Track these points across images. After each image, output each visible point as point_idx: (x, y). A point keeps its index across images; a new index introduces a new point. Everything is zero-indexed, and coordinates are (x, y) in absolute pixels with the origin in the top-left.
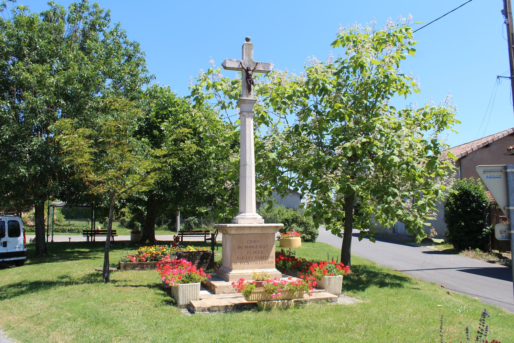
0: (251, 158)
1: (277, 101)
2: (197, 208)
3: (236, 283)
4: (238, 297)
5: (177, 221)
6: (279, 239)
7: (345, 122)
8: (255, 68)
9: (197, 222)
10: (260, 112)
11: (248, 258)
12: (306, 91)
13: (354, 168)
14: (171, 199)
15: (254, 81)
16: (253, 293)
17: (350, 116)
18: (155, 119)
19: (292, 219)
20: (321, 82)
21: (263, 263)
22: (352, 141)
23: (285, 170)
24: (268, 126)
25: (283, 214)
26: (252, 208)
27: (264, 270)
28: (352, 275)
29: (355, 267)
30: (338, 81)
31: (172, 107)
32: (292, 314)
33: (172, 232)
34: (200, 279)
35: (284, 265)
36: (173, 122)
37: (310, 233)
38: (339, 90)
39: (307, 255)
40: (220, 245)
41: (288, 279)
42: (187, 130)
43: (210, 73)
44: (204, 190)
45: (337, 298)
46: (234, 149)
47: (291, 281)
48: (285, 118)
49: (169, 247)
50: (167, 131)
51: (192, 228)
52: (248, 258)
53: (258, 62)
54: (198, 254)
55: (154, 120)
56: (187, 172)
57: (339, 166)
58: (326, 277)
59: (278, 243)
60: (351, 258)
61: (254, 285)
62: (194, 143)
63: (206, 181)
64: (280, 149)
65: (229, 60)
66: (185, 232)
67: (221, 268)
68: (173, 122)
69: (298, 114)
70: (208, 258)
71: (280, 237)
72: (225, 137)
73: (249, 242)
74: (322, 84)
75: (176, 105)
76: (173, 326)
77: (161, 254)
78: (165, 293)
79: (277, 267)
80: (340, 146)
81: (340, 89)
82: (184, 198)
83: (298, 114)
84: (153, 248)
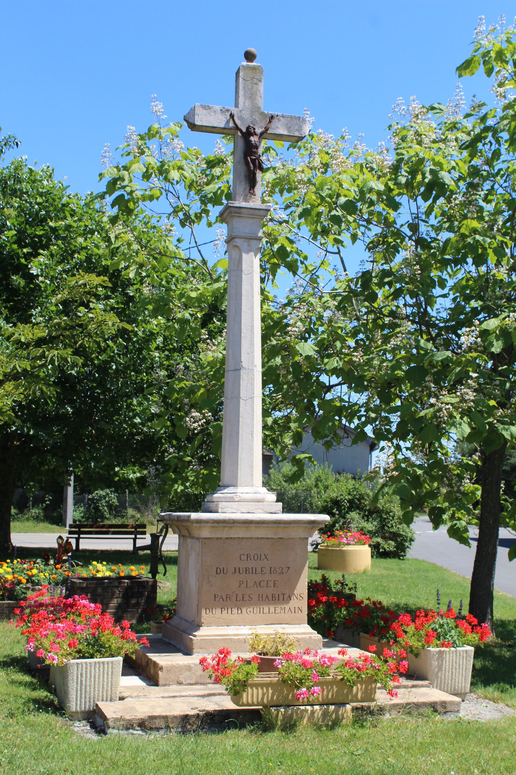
0: (251, 353)
1: (319, 215)
2: (117, 469)
3: (209, 661)
4: (214, 695)
5: (66, 498)
6: (316, 548)
7: (488, 267)
8: (267, 129)
9: (115, 501)
10: (276, 240)
11: (240, 597)
12: (393, 190)
13: (505, 382)
14: (52, 447)
15: (263, 158)
16: (252, 686)
17: (499, 252)
18: (15, 246)
19: (349, 501)
20: (428, 167)
21: (278, 610)
22: (504, 315)
23: (334, 380)
24: (295, 273)
25: (326, 488)
26: (252, 475)
27: (280, 629)
28: (496, 645)
29: (503, 624)
30: (473, 163)
31: (57, 218)
32: (348, 741)
33: (54, 526)
34: (122, 648)
35: (329, 614)
36: (62, 255)
37: (394, 536)
38: (472, 186)
39: (385, 591)
40: (173, 561)
41: (339, 653)
42: (94, 279)
43: (154, 136)
44: (135, 424)
45: (458, 704)
46: (211, 325)
47: (346, 658)
48: (339, 253)
49: (47, 564)
50: (46, 277)
51: (103, 517)
52: (240, 597)
53: (275, 113)
54: (116, 584)
55: (13, 250)
56: (95, 380)
57: (471, 378)
58: (433, 649)
59: (313, 559)
60: (495, 603)
61: (255, 665)
62: (113, 309)
63: (140, 404)
64: (323, 332)
65: (204, 107)
66: (85, 526)
67: (175, 621)
68: (62, 255)
69: (372, 247)
70: (141, 595)
71: (317, 544)
72: (189, 298)
73: (243, 557)
74: (432, 171)
75: (67, 214)
76: (53, 765)
77: (24, 581)
78: (35, 681)
79: (312, 623)
80: (473, 328)
81: (478, 185)
82: (86, 444)
83: (372, 247)
84: (5, 565)
